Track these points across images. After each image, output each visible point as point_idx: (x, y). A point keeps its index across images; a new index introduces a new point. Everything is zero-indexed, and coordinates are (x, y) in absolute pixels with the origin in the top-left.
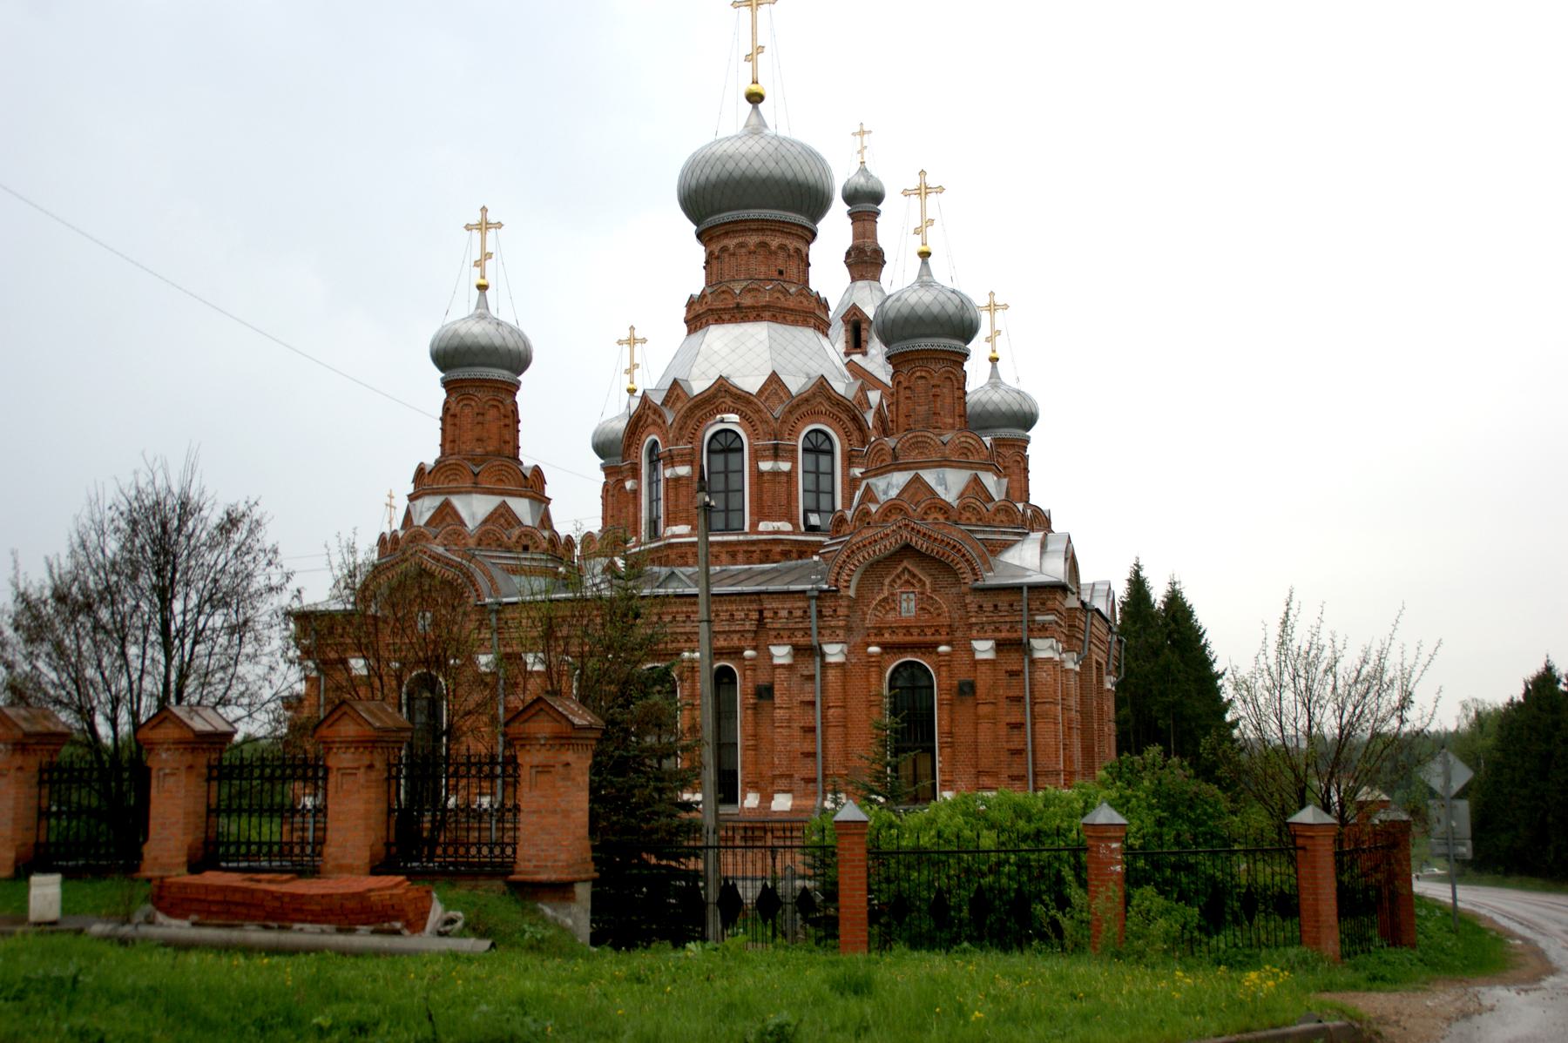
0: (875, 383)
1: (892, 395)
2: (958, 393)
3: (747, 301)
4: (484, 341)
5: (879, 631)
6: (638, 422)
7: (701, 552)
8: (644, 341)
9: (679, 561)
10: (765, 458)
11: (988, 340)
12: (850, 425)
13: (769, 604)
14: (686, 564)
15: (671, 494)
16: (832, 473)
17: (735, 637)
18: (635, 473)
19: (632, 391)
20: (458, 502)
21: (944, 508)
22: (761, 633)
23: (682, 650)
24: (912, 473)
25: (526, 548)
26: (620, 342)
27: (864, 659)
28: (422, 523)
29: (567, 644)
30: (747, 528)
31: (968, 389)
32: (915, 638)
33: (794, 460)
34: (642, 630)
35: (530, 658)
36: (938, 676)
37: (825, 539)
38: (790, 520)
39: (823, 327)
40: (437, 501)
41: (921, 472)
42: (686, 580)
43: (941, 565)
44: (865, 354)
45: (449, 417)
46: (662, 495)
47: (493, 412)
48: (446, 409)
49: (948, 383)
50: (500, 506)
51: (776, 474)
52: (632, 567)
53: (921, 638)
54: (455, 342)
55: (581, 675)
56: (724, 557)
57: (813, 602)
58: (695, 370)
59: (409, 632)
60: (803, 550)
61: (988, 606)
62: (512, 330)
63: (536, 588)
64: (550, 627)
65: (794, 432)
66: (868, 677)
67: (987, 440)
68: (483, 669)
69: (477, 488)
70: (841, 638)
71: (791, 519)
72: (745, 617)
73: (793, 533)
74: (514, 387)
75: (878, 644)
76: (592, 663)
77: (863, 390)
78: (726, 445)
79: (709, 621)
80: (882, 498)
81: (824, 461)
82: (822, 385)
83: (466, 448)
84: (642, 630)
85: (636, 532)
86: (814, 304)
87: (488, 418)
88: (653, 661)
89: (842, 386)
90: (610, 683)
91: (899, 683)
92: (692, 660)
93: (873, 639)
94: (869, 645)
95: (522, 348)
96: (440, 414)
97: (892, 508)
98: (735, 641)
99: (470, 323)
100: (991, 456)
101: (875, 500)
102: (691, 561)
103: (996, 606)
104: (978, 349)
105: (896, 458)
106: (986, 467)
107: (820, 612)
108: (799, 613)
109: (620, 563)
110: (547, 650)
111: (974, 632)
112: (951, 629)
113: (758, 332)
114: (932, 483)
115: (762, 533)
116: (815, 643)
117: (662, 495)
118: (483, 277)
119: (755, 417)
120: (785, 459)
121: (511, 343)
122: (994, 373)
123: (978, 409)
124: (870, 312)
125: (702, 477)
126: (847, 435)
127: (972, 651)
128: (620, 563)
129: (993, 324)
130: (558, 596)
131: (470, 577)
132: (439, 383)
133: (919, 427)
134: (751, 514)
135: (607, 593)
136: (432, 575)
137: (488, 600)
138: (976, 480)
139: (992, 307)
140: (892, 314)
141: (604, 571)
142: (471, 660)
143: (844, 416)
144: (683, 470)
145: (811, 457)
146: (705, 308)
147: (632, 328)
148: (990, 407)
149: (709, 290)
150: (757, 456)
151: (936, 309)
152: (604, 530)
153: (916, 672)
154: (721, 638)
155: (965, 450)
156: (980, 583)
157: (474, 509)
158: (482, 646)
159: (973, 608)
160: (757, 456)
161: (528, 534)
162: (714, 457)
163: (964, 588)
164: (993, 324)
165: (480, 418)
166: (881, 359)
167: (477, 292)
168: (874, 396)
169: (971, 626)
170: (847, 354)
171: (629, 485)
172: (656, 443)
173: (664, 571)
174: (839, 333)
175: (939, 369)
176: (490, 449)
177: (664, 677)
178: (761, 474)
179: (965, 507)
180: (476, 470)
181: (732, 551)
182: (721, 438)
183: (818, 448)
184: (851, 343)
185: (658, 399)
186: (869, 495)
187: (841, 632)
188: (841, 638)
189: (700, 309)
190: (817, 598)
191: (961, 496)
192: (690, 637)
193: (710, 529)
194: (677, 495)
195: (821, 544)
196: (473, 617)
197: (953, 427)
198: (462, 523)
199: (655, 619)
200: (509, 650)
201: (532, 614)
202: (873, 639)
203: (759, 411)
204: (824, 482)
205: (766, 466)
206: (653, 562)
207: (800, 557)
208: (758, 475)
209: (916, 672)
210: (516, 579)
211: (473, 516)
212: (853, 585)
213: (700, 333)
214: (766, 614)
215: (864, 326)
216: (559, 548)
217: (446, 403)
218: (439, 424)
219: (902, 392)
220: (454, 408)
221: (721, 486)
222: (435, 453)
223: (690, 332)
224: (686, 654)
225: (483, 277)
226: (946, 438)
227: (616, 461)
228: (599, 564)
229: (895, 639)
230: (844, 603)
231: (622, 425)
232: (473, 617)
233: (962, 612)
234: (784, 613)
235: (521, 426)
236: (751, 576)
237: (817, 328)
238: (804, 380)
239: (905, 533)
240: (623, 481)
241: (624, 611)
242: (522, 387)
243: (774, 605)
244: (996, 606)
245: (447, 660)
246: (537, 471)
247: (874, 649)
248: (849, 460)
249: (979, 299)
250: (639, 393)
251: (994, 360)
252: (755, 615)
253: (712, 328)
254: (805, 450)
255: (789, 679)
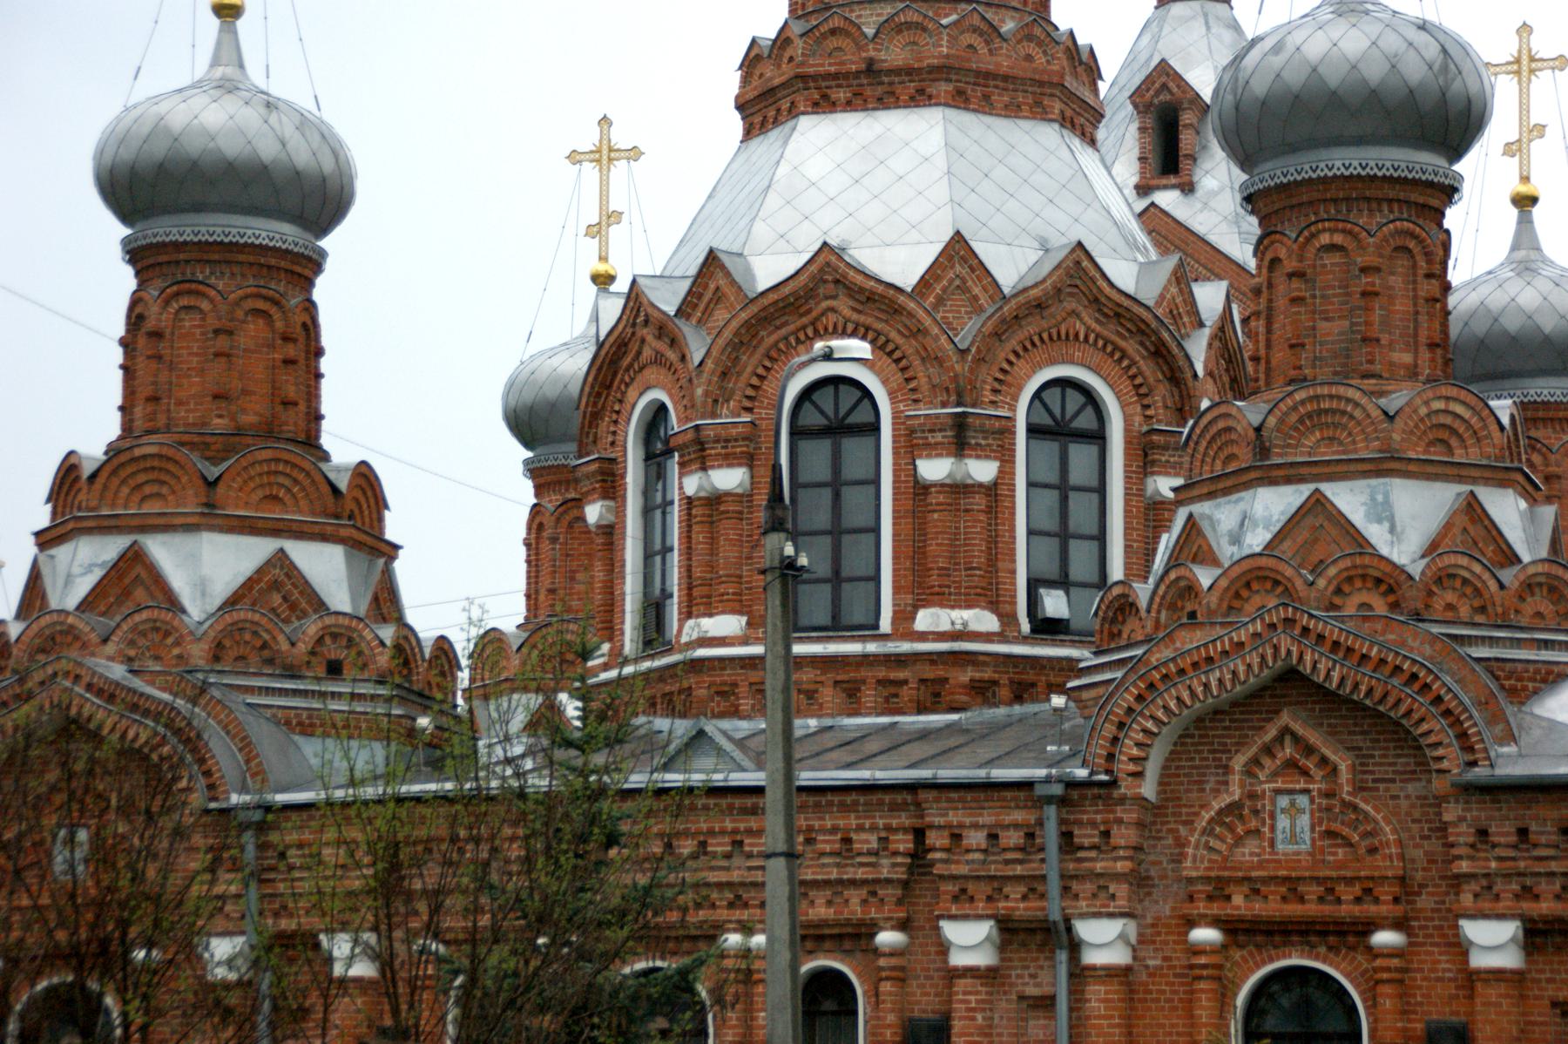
0: (1212, 261)
1: (1255, 292)
2: (1428, 288)
3: (894, 54)
4: (232, 148)
5: (1219, 889)
6: (615, 361)
7: (773, 681)
8: (634, 154)
9: (718, 704)
10: (933, 450)
11: (1510, 150)
12: (1148, 368)
13: (938, 815)
14: (735, 713)
15: (699, 537)
16: (1101, 490)
17: (855, 897)
18: (610, 485)
19: (603, 281)
20: (164, 552)
21: (1387, 579)
22: (921, 887)
23: (719, 928)
24: (1305, 490)
25: (334, 669)
26: (574, 157)
27: (1180, 960)
28: (71, 602)
29: (435, 910)
30: (885, 625)
31: (1456, 276)
32: (1312, 909)
33: (1005, 456)
34: (623, 876)
35: (341, 946)
36: (1372, 1006)
37: (1083, 655)
38: (994, 605)
39: (1082, 120)
40: (110, 548)
41: (1328, 489)
42: (733, 753)
43: (1378, 724)
44: (1188, 188)
45: (141, 336)
46: (675, 539)
47: (255, 327)
48: (136, 317)
49: (1402, 263)
50: (269, 563)
51: (959, 489)
52: (602, 717)
53: (1327, 909)
54: (159, 150)
55: (467, 990)
56: (827, 695)
57: (1051, 811)
58: (759, 227)
59: (31, 878)
60: (1026, 681)
61: (1503, 832)
62: (305, 122)
63: (361, 766)
64: (395, 866)
65: (1006, 385)
66: (1190, 1003)
67: (1503, 408)
68: (221, 973)
69: (213, 516)
70: (1122, 903)
71: (996, 601)
72: (878, 847)
73: (1000, 637)
74: (307, 267)
75: (1215, 922)
76: (497, 958)
77: (1182, 279)
78: (837, 415)
79: (790, 855)
80: (1228, 553)
81: (1081, 457)
82: (1079, 270)
83: (186, 415)
84: (623, 876)
85: (610, 630)
86: (1061, 63)
87: (243, 341)
88: (649, 952)
89: (1129, 269)
90: (542, 1009)
91: (1271, 1023)
92: (746, 953)
93: (1201, 907)
94: (1192, 923)
95: (328, 165)
96: (119, 328)
97: (1254, 577)
98: (854, 907)
99: (199, 101)
100: (1512, 447)
101: (1208, 557)
102: (746, 704)
103: (1523, 832)
104: (1483, 173)
105: (1263, 451)
106: (1500, 477)
107: (1067, 837)
108: (1013, 838)
109: (571, 708)
110: (384, 925)
111: (1467, 899)
112: (1406, 887)
113: (919, 136)
114: (1357, 516)
115: (923, 636)
116: (1055, 915)
117: (675, 539)
118: (603, 258)
119: (909, 347)
120: (982, 453)
121: (302, 154)
122: (1525, 234)
123: (1480, 328)
124: (1203, 80)
125: (776, 497)
126: (1141, 392)
127: (1461, 948)
128: (571, 708)
129: (1524, 108)
130: (416, 788)
131: (193, 742)
132: (117, 252)
133: (1324, 373)
134: (897, 589)
135: (539, 783)
136: (96, 737)
137: (235, 799)
138: (1473, 510)
139: (1525, 65)
140: (1260, 87)
141: (531, 726)
142: (189, 952)
143: (1131, 346)
144: (729, 478)
145: (1050, 448)
146: (788, 71)
147: (605, 121)
148: (1512, 324)
149: (797, 28)
150: (912, 444)
151: (1374, 72)
152: (532, 624)
153: (1320, 999)
154: (820, 897)
155: (1443, 433)
156: (1480, 773)
157: (205, 569)
158: (217, 914)
159: (1463, 835)
160: (912, 444)
161: (342, 632)
162: (805, 446)
163: (1439, 785)
164: (1524, 108)
165: (222, 343)
166: (1230, 202)
167: (215, 22)
168: (1210, 297)
169: (1458, 881)
170: (1143, 189)
171: (594, 512)
172: (661, 409)
173: (683, 727)
174: (1123, 135)
175: (1378, 225)
176: (248, 419)
177: (675, 994)
178: (922, 489)
179: (1443, 578)
180: (213, 472)
181: (849, 682)
182: (825, 398)
183: (1066, 425)
184: (1154, 160)
185: (667, 301)
186: (1194, 545)
187: (1121, 890)
188: (1122, 903)
189: (774, 75)
190: (1062, 802)
191: (1432, 549)
192: (743, 896)
193: (794, 626)
194: (713, 540)
195: (1070, 667)
196: (198, 840)
197: (1413, 373)
198: (173, 603)
199: (657, 849)
200: (287, 924)
201: (354, 833)
202: (1201, 907)
203: (919, 332)
204: (1081, 511)
205: (934, 469)
206: (652, 707)
207: (1018, 699)
208: (915, 492)
209: (1320, 999)
210: (311, 749)
211: (202, 587)
212: (1152, 769)
213: (775, 135)
214: (933, 838)
215: (1187, 117)
216: (419, 671)
217: (135, 301)
218: (117, 355)
219: (1283, 289)
220: (156, 316)
221: (822, 519)
222: (111, 428)
223: (748, 134)
224: (733, 939)
225: (603, 258)
226: (1394, 402)
227: (564, 454)
228: (522, 706)
229: (1259, 908)
230: (1129, 814)
231: (578, 364)
232: (198, 840)
233: (1434, 845)
234: (976, 838)
235: (325, 364)
236: (895, 743)
237: (1067, 123)
238: (1034, 256)
239: (1285, 643)
240: (579, 503)
241: (580, 825)
242: (330, 265)
243: (953, 818)
244: (1523, 832)
245: (127, 951)
246: (365, 476)
247: (1205, 935)
248: (1144, 456)
249: (1489, 43)
250: (621, 285)
251: (1524, 203)
252: (904, 843)
253: (805, 122)
254: (1033, 431)
255: (988, 1006)
